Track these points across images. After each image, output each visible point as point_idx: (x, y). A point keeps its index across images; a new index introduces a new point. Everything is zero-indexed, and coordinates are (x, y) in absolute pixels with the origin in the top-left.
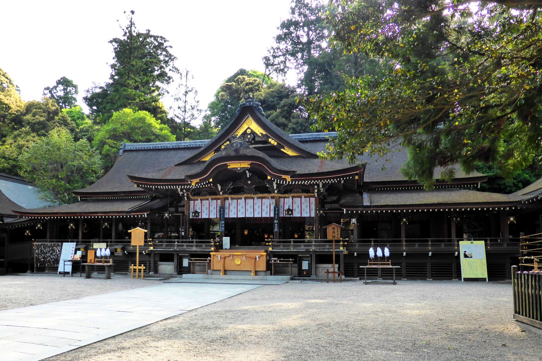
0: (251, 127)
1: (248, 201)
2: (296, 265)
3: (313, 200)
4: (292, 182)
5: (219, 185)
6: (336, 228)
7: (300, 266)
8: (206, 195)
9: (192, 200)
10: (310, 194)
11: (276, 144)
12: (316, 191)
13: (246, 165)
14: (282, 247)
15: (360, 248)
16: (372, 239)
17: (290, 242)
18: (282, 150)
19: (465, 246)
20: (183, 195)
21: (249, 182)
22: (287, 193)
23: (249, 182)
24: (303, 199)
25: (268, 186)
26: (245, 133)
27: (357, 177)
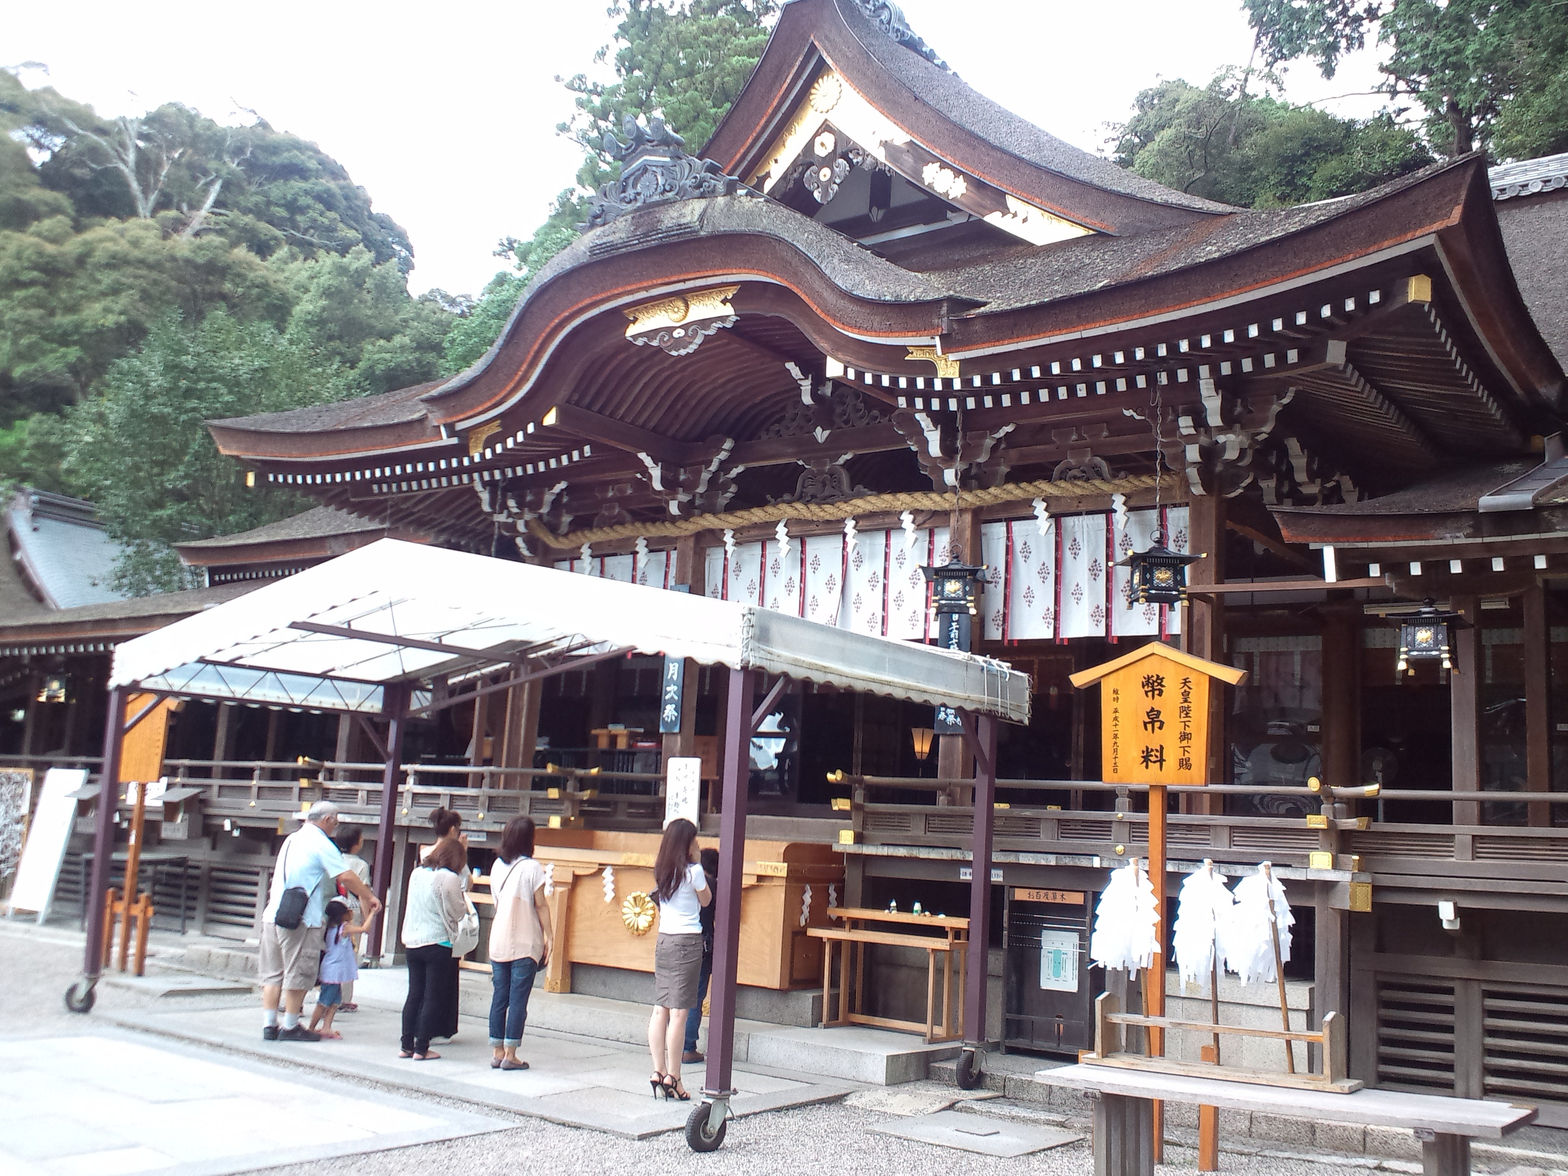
0: (836, 122)
1: (815, 547)
5: (642, 456)
8: (1091, 474)
12: (1193, 453)
14: (917, 830)
15: (1488, 865)
18: (994, 219)
19: (1332, 344)
20: (512, 527)
21: (821, 435)
22: (761, 503)
23: (821, 435)
26: (806, 160)
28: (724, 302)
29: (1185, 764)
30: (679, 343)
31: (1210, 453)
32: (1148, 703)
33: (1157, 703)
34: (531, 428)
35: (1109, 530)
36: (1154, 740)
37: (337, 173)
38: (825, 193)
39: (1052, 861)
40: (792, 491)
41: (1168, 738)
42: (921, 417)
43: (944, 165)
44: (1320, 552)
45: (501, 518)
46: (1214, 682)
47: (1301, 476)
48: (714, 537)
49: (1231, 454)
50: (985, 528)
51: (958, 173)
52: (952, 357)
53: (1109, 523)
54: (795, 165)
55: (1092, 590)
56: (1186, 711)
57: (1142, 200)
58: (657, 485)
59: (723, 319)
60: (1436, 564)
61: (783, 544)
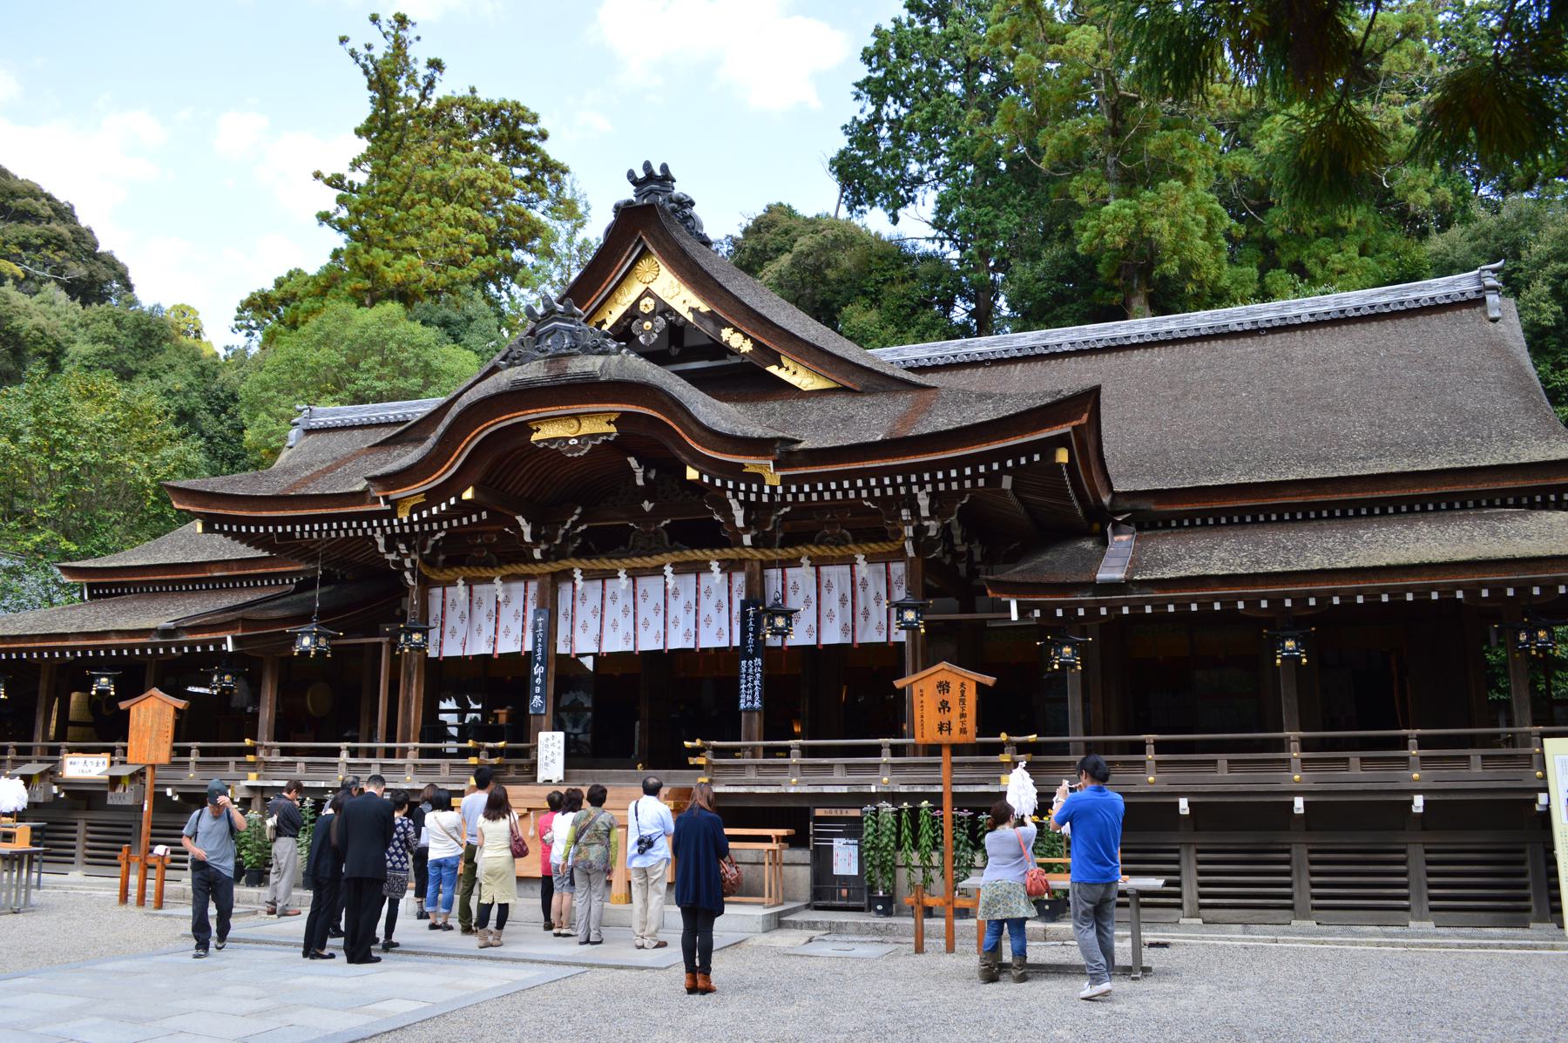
0: (654, 287)
1: (643, 582)
2: (803, 855)
3: (898, 569)
4: (787, 490)
5: (521, 520)
6: (955, 688)
7: (822, 859)
8: (840, 541)
9: (436, 584)
10: (886, 547)
11: (747, 347)
12: (909, 531)
13: (599, 425)
16: (1150, 738)
17: (876, 751)
18: (773, 369)
20: (400, 564)
21: (647, 506)
23: (647, 506)
24: (863, 568)
25: (717, 517)
26: (633, 314)
27: (1062, 456)
28: (609, 423)
29: (963, 731)
30: (574, 448)
31: (920, 531)
32: (940, 697)
33: (946, 697)
34: (453, 501)
35: (853, 575)
36: (945, 718)
37: (64, 213)
38: (648, 338)
39: (845, 790)
40: (626, 545)
41: (954, 716)
42: (734, 503)
43: (736, 330)
44: (1008, 604)
45: (391, 557)
46: (978, 684)
47: (957, 541)
48: (568, 575)
49: (932, 533)
50: (767, 572)
51: (746, 337)
52: (779, 474)
53: (852, 571)
54: (625, 315)
55: (842, 615)
56: (963, 701)
57: (878, 373)
58: (528, 539)
59: (608, 434)
60: (1070, 609)
61: (623, 581)
